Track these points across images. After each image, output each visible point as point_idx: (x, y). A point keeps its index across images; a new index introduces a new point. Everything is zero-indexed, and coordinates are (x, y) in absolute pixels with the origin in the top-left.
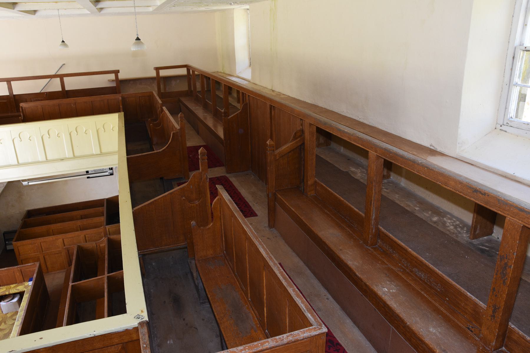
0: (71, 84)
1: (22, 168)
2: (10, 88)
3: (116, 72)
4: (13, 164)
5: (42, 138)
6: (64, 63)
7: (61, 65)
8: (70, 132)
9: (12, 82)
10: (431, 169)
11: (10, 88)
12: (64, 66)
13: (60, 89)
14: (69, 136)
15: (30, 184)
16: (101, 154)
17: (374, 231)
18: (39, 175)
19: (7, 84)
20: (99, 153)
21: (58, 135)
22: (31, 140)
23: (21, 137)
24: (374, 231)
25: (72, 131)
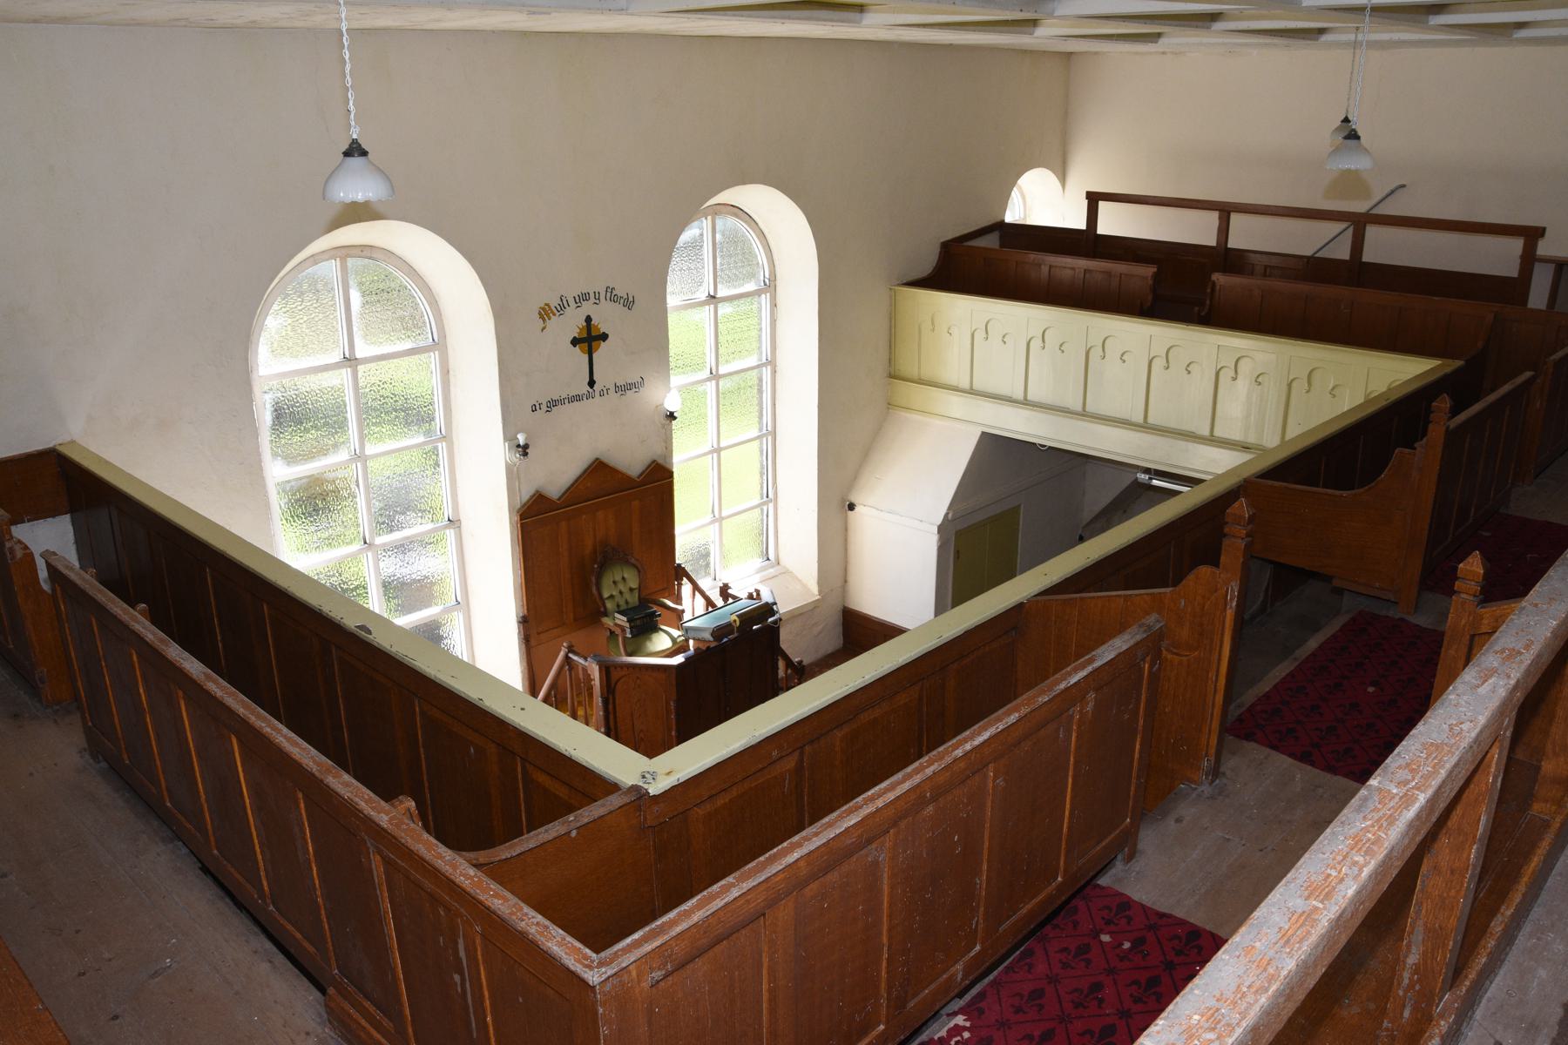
0: (1383, 247)
1: (1025, 413)
2: (1224, 230)
3: (1532, 235)
4: (1133, 420)
5: (973, 335)
6: (1405, 183)
7: (1393, 187)
8: (1152, 356)
9: (1101, 204)
10: (263, 477)
11: (1224, 230)
12: (1401, 190)
13: (1082, 225)
14: (1285, 388)
15: (1155, 482)
16: (1084, 414)
17: (1407, 1014)
18: (1084, 447)
19: (1220, 218)
20: (1079, 408)
21: (1260, 379)
22: (1063, 352)
23: (1239, 370)
24: (1407, 1014)
25: (1095, 346)
